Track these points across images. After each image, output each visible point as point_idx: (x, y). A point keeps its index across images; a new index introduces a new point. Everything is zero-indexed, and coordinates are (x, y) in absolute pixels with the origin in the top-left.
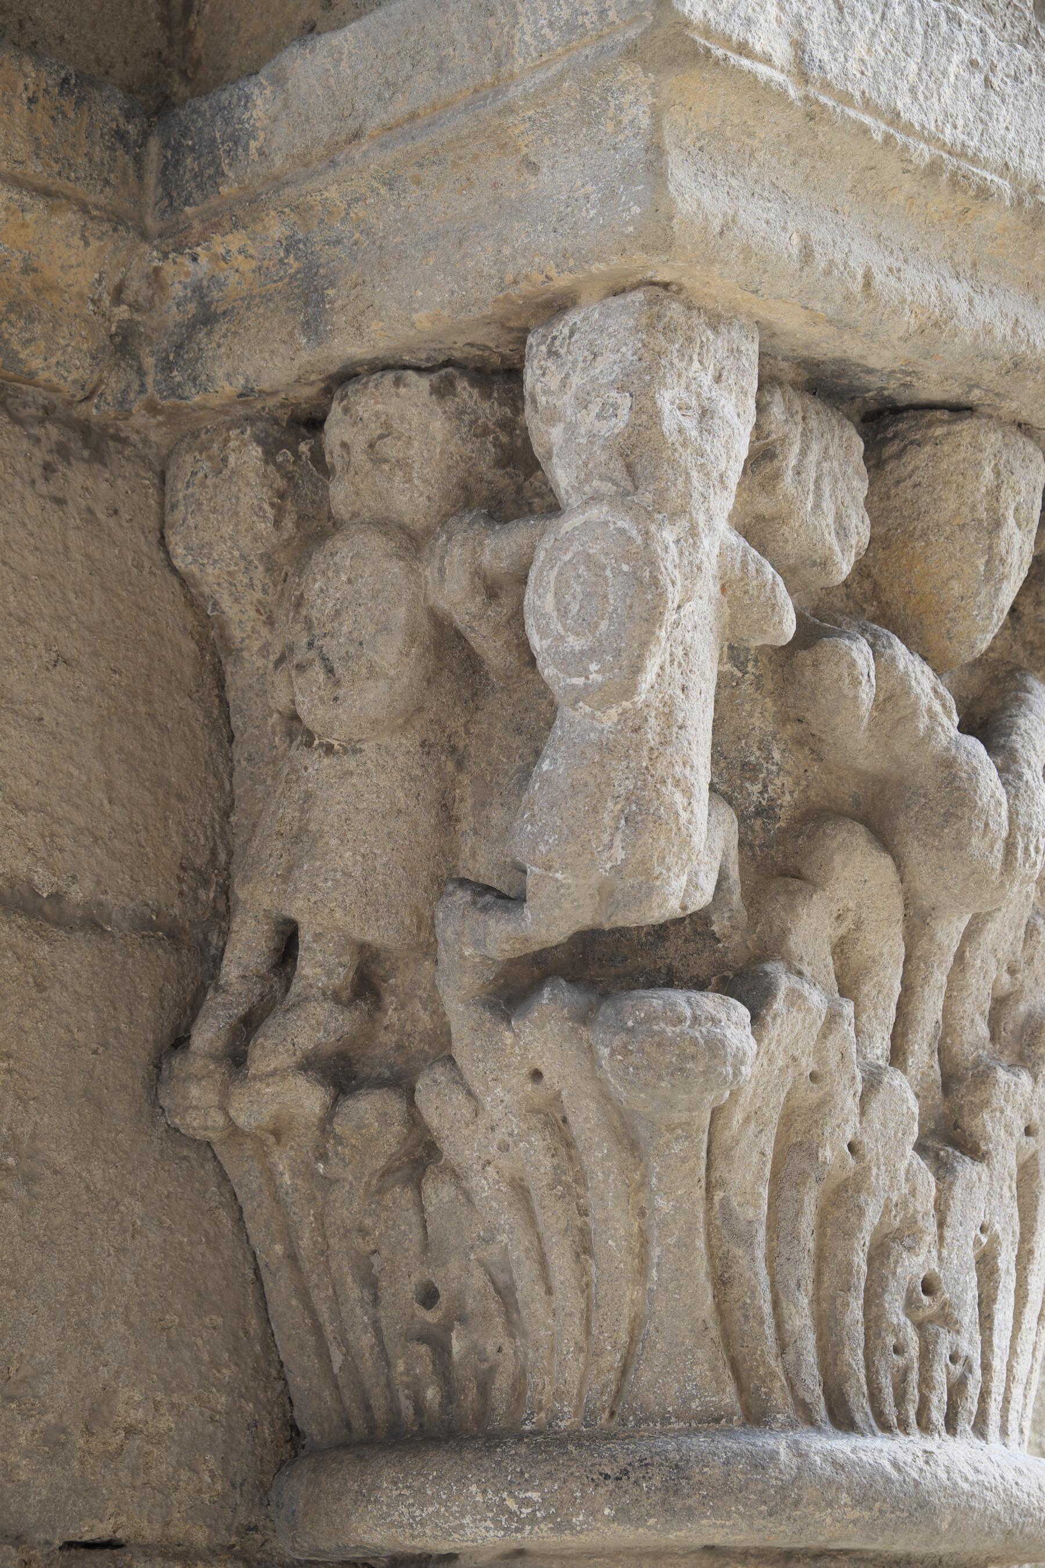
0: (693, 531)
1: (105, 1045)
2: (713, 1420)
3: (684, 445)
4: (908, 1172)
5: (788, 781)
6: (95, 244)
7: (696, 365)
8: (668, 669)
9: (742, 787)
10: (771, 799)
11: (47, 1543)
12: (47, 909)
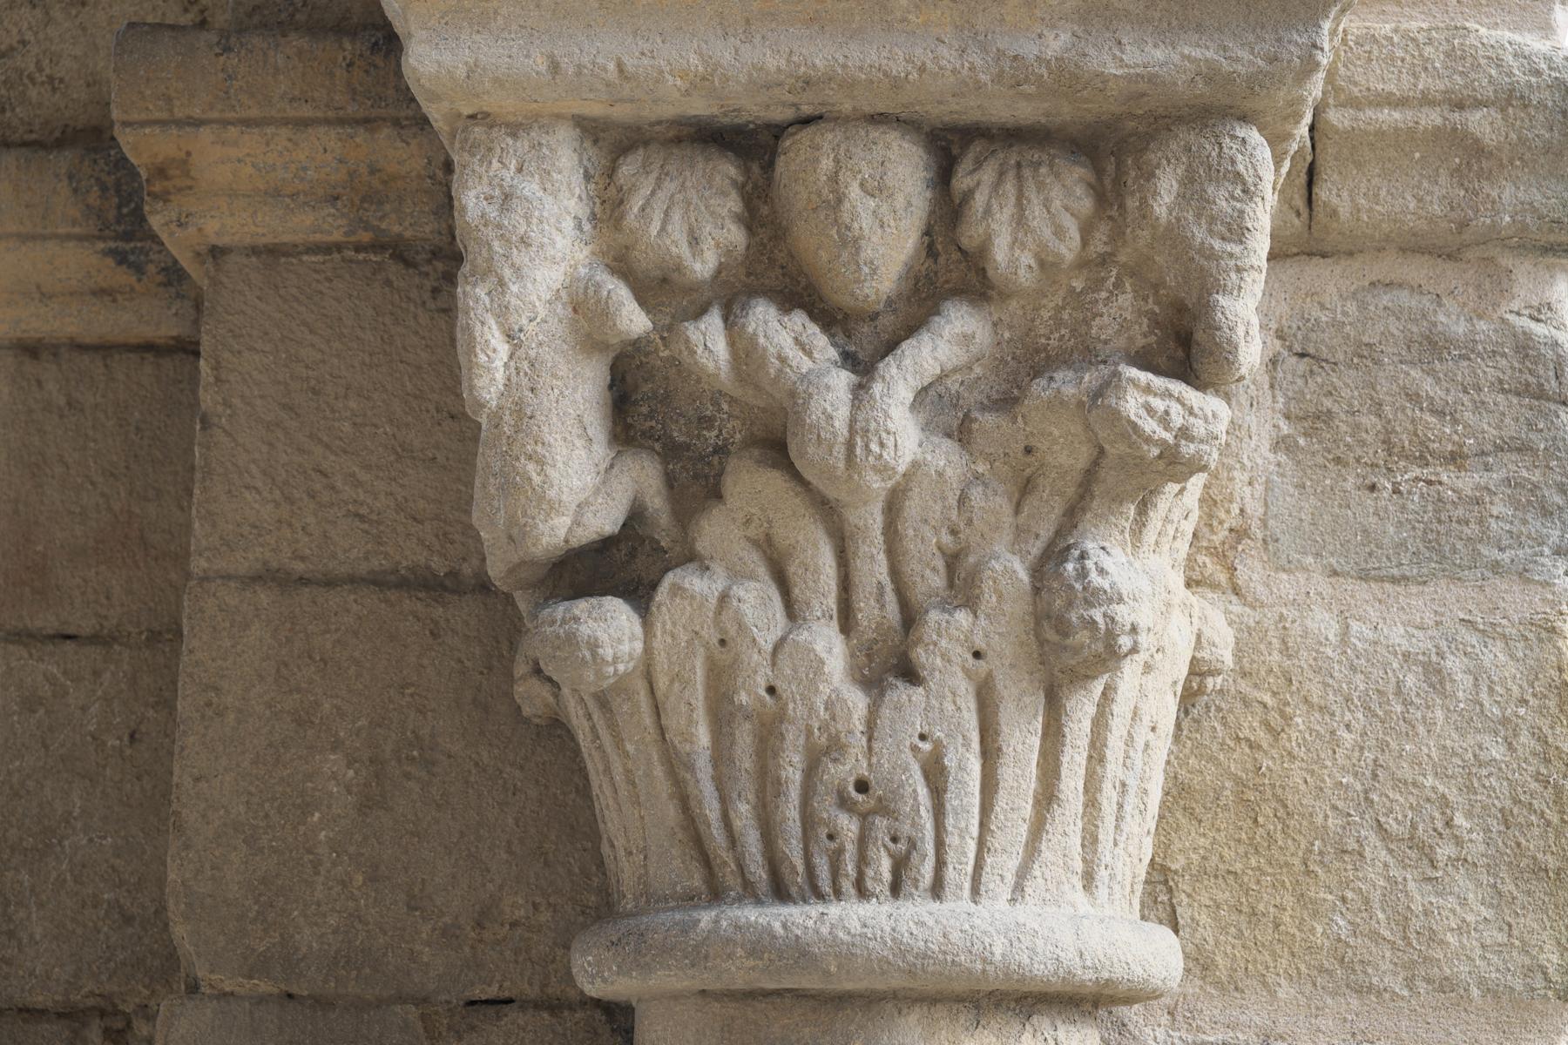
0: (502, 283)
1: (490, 669)
2: (690, 899)
3: (486, 225)
4: (826, 703)
5: (737, 423)
6: (414, 142)
7: (496, 164)
8: (514, 379)
9: (698, 436)
10: (725, 439)
11: (448, 1002)
12: (447, 583)
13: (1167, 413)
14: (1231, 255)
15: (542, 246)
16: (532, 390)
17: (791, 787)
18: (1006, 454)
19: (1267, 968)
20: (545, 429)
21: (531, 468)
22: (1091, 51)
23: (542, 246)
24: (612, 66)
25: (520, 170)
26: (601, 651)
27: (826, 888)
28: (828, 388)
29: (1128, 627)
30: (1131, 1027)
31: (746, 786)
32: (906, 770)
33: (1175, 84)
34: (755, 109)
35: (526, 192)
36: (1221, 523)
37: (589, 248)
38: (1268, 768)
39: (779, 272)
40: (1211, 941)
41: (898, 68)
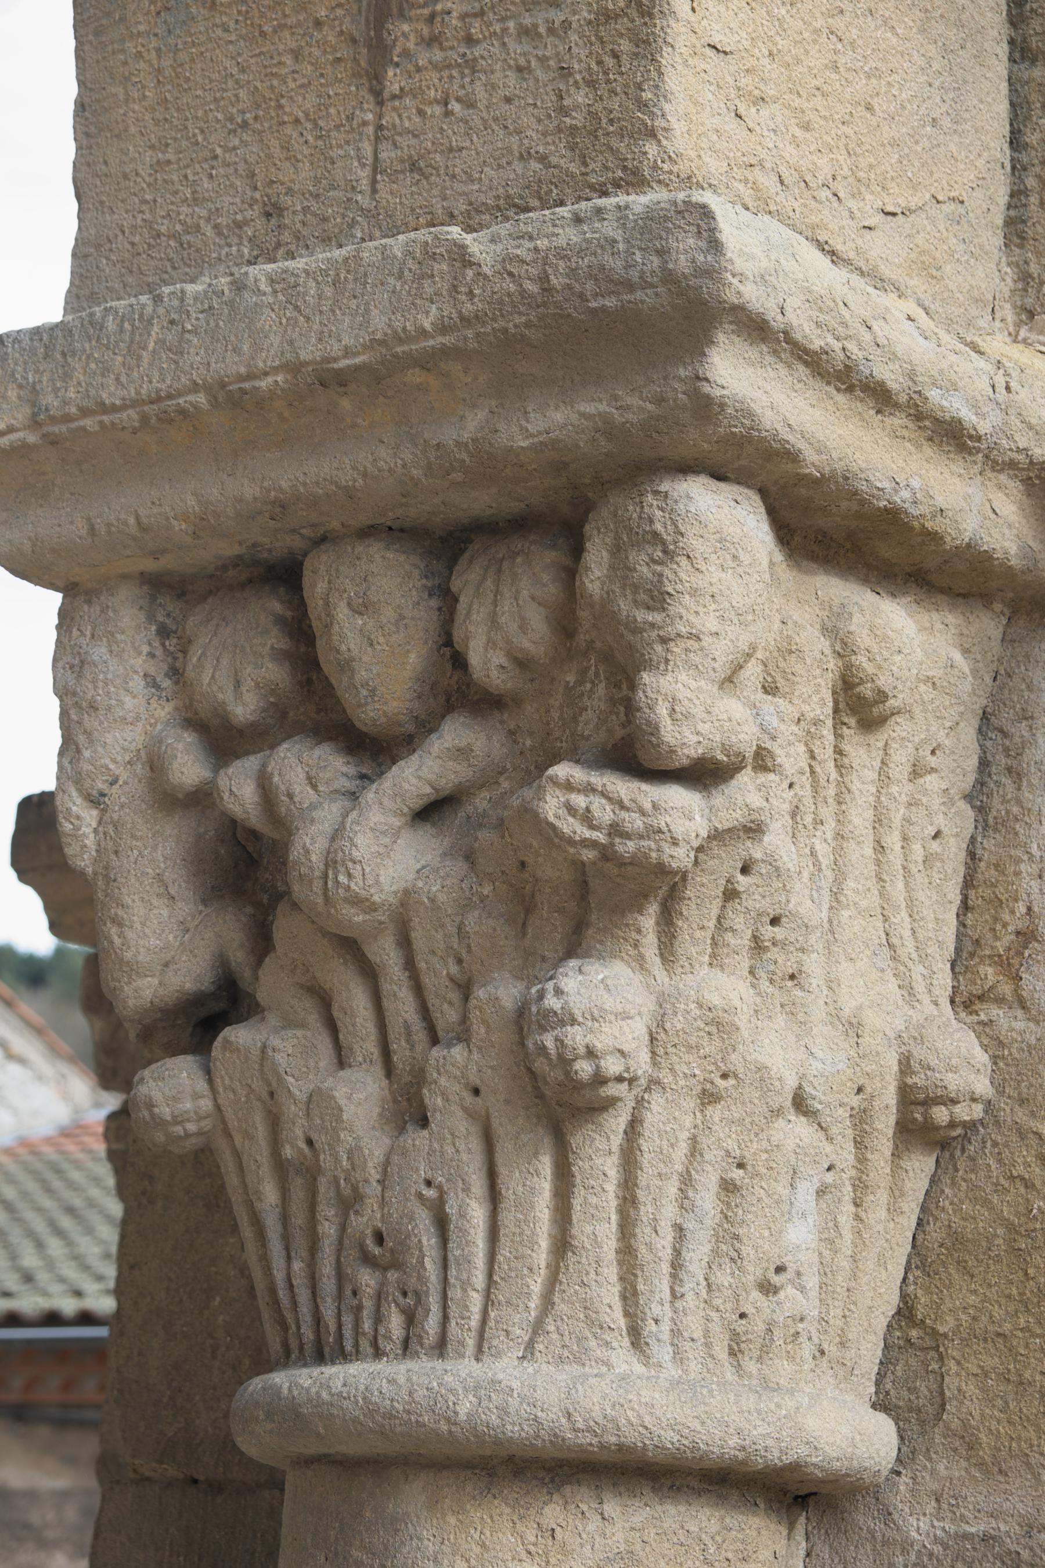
13: (588, 809)
14: (653, 625)
15: (109, 709)
16: (116, 852)
17: (327, 1242)
18: (503, 872)
19: (1031, 1446)
20: (124, 890)
21: (114, 931)
22: (501, 426)
23: (109, 709)
24: (132, 521)
25: (93, 636)
26: (156, 1110)
27: (348, 1346)
28: (313, 821)
29: (582, 1051)
30: (896, 1516)
31: (300, 1243)
32: (412, 1219)
33: (578, 446)
34: (284, 544)
35: (95, 658)
36: (1005, 925)
37: (172, 704)
38: (1039, 1209)
39: (316, 706)
40: (976, 1414)
41: (346, 478)
